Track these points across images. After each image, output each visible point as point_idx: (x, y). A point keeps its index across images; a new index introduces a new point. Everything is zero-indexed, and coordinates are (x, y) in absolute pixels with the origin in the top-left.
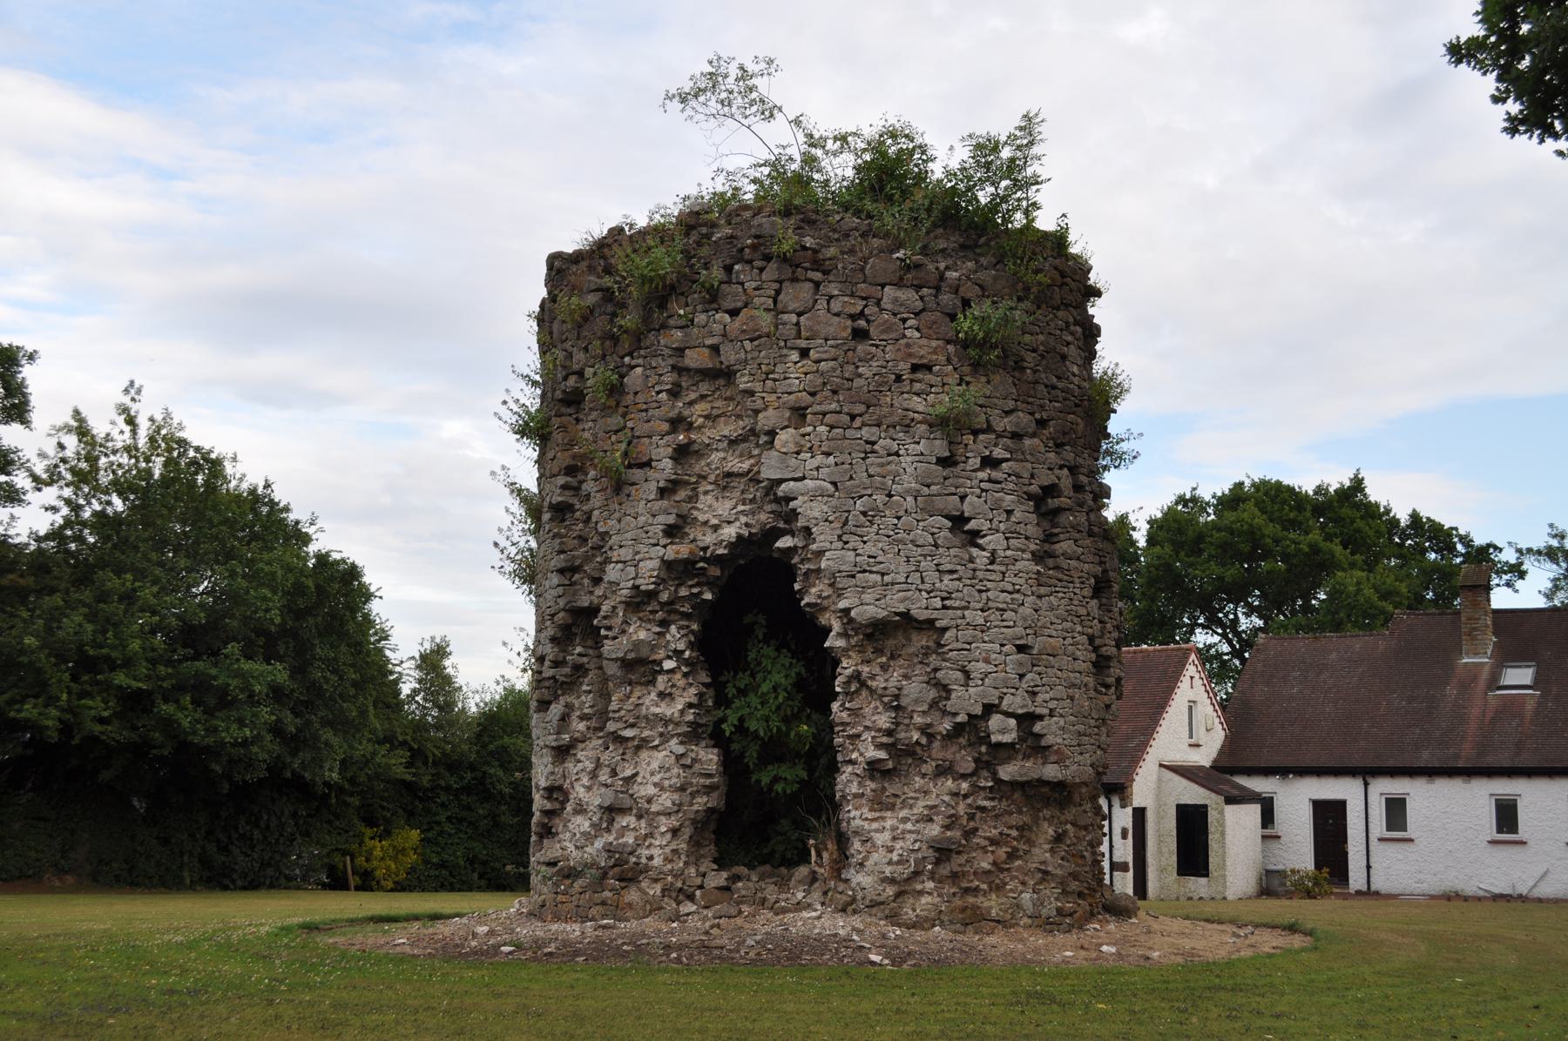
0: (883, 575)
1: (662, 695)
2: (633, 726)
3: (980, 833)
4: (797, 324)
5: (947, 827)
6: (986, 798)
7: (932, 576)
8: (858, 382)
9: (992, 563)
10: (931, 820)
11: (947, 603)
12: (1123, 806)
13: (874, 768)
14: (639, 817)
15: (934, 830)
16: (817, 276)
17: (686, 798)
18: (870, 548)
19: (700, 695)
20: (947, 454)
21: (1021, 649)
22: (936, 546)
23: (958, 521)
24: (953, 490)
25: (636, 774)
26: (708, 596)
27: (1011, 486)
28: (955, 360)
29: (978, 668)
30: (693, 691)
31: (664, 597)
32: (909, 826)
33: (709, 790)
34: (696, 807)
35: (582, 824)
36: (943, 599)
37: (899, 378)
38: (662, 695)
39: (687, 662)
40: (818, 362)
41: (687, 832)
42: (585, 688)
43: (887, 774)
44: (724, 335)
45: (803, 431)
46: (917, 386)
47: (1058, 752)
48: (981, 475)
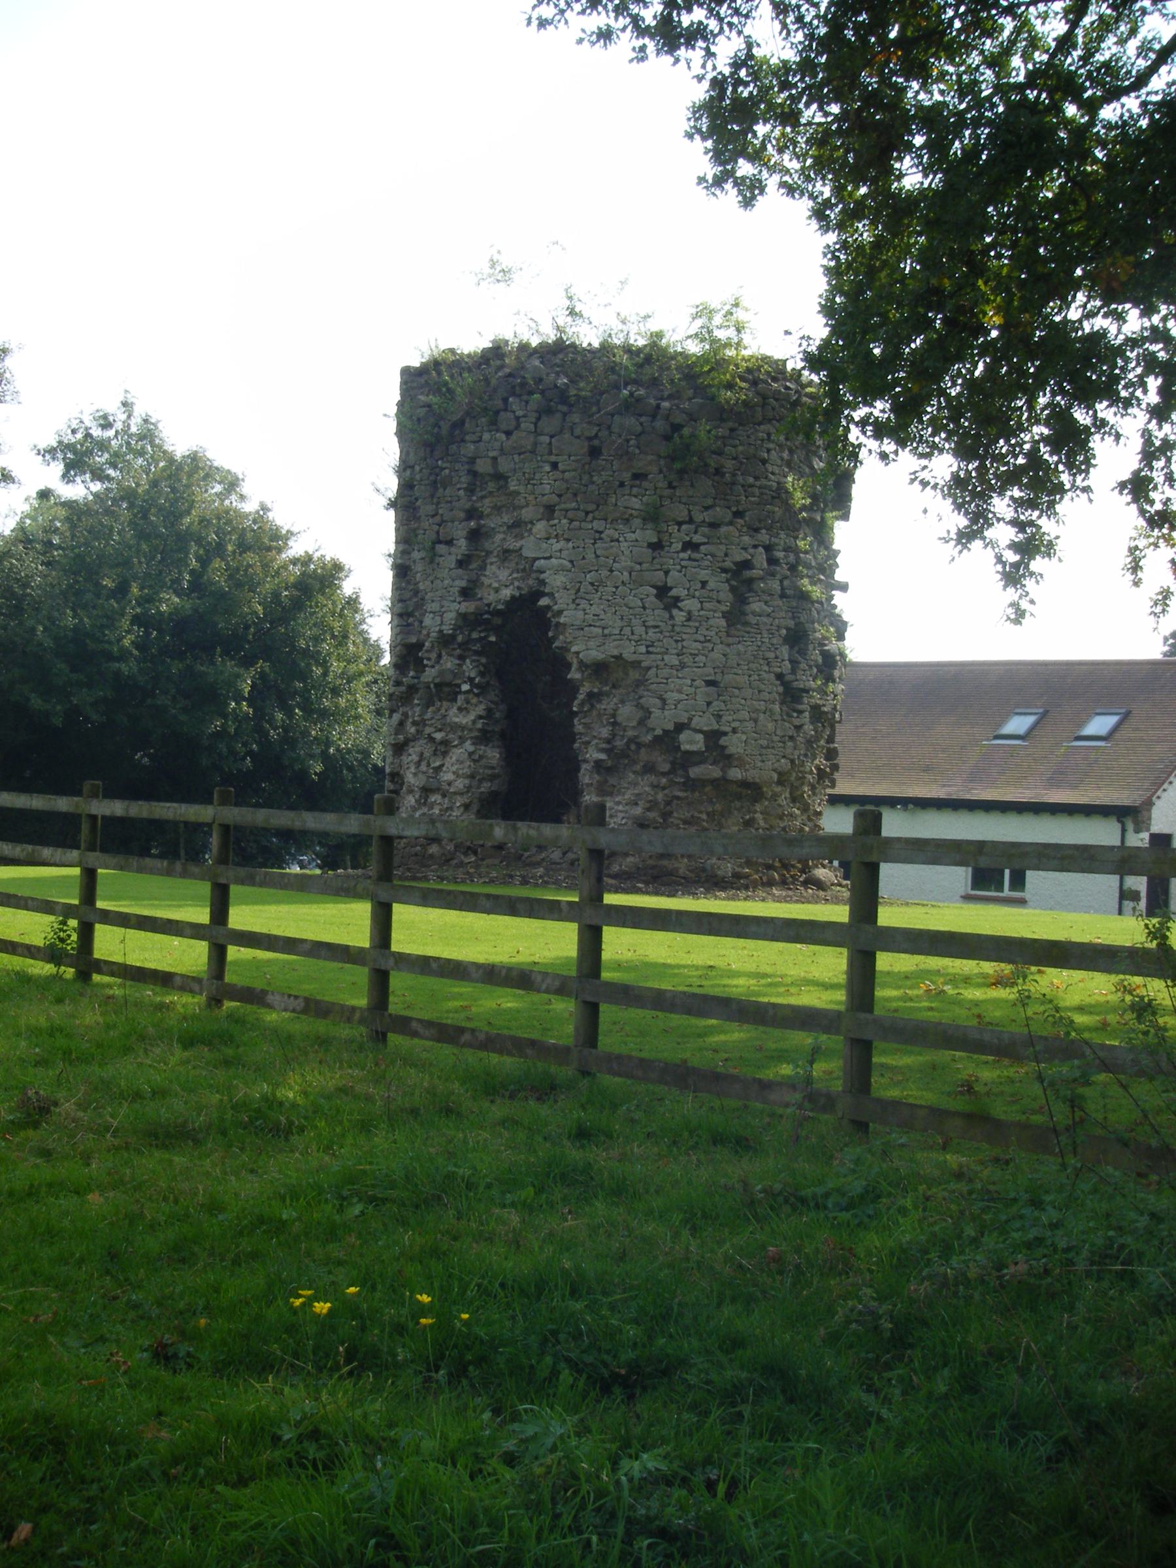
0: (604, 628)
1: (460, 709)
2: (440, 730)
3: (675, 814)
4: (550, 443)
5: (648, 809)
6: (681, 790)
7: (640, 630)
8: (591, 487)
9: (689, 620)
10: (636, 804)
11: (651, 649)
12: (1137, 831)
13: (598, 764)
14: (444, 796)
15: (638, 811)
16: (565, 409)
17: (475, 783)
18: (595, 609)
19: (489, 711)
20: (655, 540)
21: (711, 683)
22: (644, 608)
23: (662, 591)
24: (658, 567)
25: (443, 765)
26: (493, 639)
27: (707, 563)
28: (664, 469)
29: (672, 697)
30: (482, 707)
31: (460, 638)
32: (620, 808)
33: (492, 778)
34: (482, 790)
35: (411, 800)
36: (647, 647)
37: (622, 485)
38: (460, 709)
39: (477, 686)
40: (563, 472)
41: (475, 807)
42: (416, 701)
43: (609, 770)
44: (502, 450)
45: (552, 523)
46: (635, 490)
47: (739, 759)
48: (682, 555)
